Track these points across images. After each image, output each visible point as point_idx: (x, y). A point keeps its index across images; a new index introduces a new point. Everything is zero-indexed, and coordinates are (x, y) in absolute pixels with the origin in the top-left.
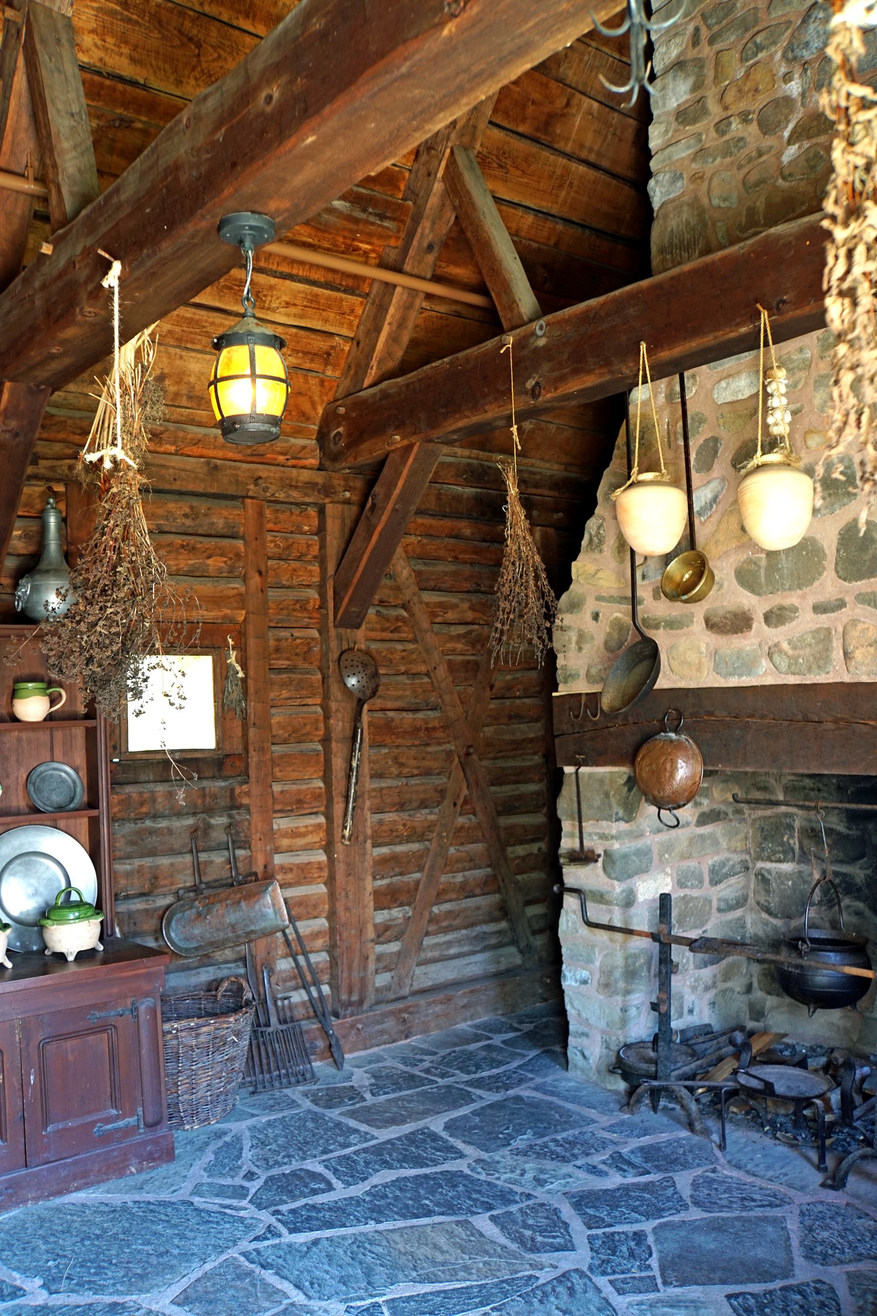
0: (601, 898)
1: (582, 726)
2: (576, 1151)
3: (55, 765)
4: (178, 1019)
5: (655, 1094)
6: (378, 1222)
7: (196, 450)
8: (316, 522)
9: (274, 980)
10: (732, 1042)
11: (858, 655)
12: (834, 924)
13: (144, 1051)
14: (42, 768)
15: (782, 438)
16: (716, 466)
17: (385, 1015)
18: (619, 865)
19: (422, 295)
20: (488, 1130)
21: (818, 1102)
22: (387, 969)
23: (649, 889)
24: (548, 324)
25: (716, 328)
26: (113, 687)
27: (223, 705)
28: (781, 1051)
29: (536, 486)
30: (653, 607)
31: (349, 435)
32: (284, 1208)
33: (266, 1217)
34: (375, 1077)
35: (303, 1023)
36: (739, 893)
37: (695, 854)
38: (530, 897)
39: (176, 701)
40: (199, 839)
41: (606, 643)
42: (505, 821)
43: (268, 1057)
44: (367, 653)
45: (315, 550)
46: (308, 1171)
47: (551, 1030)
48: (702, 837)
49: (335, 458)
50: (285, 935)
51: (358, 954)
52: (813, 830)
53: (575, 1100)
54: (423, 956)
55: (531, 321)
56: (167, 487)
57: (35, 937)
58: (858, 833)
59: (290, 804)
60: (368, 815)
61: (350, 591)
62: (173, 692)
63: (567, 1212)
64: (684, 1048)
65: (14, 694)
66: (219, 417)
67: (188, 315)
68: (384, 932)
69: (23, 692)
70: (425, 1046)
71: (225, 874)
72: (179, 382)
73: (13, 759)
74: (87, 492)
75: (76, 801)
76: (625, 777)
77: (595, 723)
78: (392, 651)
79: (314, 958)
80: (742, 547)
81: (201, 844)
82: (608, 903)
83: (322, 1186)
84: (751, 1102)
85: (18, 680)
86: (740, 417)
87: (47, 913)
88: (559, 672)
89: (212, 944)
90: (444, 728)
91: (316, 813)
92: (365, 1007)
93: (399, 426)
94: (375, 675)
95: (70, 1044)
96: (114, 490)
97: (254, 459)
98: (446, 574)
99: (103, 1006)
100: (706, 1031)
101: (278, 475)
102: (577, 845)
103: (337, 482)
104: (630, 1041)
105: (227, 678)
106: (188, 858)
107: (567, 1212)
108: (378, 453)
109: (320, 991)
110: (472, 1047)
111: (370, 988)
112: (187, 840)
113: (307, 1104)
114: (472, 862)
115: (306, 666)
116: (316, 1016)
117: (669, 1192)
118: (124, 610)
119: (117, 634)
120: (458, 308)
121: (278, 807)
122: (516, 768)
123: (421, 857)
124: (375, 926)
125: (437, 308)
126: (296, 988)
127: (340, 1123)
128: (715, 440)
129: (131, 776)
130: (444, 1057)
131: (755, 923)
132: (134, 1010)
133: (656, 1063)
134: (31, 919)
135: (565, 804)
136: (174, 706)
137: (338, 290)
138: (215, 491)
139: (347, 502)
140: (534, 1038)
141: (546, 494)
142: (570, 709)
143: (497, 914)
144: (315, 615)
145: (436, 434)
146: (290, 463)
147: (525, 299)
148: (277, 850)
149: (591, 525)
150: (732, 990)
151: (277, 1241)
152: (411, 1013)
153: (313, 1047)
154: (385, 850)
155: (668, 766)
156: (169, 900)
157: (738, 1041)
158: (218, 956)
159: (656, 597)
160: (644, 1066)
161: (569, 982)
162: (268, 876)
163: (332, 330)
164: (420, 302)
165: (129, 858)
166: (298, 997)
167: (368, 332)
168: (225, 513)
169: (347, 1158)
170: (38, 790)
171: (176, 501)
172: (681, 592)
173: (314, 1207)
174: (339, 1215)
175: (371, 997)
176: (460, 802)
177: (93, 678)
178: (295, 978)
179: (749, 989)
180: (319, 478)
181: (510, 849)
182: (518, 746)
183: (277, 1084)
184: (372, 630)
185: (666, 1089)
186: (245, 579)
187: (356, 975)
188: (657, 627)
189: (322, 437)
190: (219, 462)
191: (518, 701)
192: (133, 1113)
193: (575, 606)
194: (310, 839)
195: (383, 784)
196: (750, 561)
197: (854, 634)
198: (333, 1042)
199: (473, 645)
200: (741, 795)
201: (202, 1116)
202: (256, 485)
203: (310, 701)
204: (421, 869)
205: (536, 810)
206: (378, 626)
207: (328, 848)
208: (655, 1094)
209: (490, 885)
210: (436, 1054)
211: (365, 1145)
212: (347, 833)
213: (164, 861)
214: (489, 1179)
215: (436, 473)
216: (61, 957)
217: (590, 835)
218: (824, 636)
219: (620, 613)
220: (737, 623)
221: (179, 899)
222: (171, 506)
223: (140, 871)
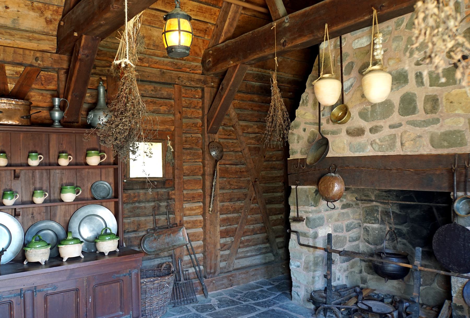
0: (305, 235)
1: (298, 171)
3: (102, 182)
4: (147, 277)
5: (325, 310)
7: (156, 66)
8: (201, 94)
9: (182, 264)
10: (355, 291)
11: (407, 144)
12: (395, 248)
13: (133, 290)
14: (97, 183)
15: (380, 60)
16: (352, 73)
17: (223, 278)
18: (312, 223)
19: (241, 8)
21: (389, 315)
22: (225, 260)
23: (323, 232)
24: (290, 18)
25: (356, 17)
26: (125, 149)
27: (165, 161)
28: (373, 296)
29: (282, 83)
30: (327, 126)
31: (213, 61)
34: (220, 301)
35: (193, 280)
36: (357, 235)
37: (340, 220)
38: (277, 235)
39: (149, 155)
40: (156, 211)
41: (308, 140)
42: (269, 206)
43: (180, 293)
44: (219, 143)
45: (200, 105)
47: (286, 285)
48: (343, 213)
49: (208, 70)
50: (187, 247)
51: (214, 255)
52: (386, 212)
53: (294, 311)
54: (238, 256)
55: (283, 17)
56: (145, 79)
57: (93, 246)
58: (404, 213)
59: (189, 198)
60: (218, 203)
61: (213, 120)
62: (148, 151)
64: (336, 293)
65: (86, 155)
66: (166, 46)
67: (153, 13)
68: (223, 247)
69: (90, 154)
70: (238, 290)
71: (165, 224)
72: (150, 39)
73: (86, 179)
74: (115, 77)
75: (110, 195)
76: (315, 190)
77: (303, 170)
78: (228, 143)
79: (198, 256)
80: (361, 104)
81: (156, 212)
82: (307, 237)
84: (363, 315)
85: (88, 150)
86: (363, 54)
87: (98, 237)
88: (290, 151)
89: (160, 250)
90: (247, 171)
91: (199, 202)
92: (216, 275)
93: (232, 58)
94: (222, 151)
95: (105, 287)
96: (126, 75)
97: (178, 70)
98: (248, 114)
99: (118, 272)
100: (344, 287)
101: (187, 76)
102: (296, 215)
103: (209, 79)
104: (315, 290)
105: (167, 151)
108: (224, 68)
109: (199, 268)
110: (256, 291)
111: (218, 267)
112: (151, 211)
113: (194, 311)
114: (256, 221)
115: (196, 147)
116: (198, 278)
118: (130, 121)
119: (127, 129)
120: (255, 13)
121: (185, 199)
122: (273, 187)
123: (238, 219)
124: (220, 244)
125: (247, 13)
126: (191, 267)
128: (352, 63)
129: (131, 187)
130: (245, 294)
131: (363, 247)
132: (130, 274)
133: (326, 298)
134: (91, 240)
135: (292, 200)
136: (147, 161)
137: (210, 5)
138: (163, 81)
139: (212, 87)
140: (278, 288)
141: (287, 86)
142: (294, 164)
143: (265, 241)
144: (200, 129)
145: (246, 61)
146: (191, 72)
147: (281, 8)
148: (185, 215)
149: (304, 96)
152: (233, 277)
153: (197, 289)
154: (224, 216)
155: (331, 186)
156: (144, 233)
157: (357, 292)
158: (162, 254)
159: (328, 122)
160: (321, 299)
161: (293, 266)
162: (181, 225)
163: (208, 21)
164: (241, 11)
165: (129, 217)
166: (192, 270)
167: (221, 22)
168: (167, 90)
170: (95, 191)
171: (149, 85)
172: (338, 120)
175: (218, 271)
176: (252, 199)
177: (117, 146)
178: (190, 263)
179: (361, 272)
180: (202, 78)
181: (270, 217)
182: (274, 179)
183: (183, 303)
184: (221, 135)
185: (330, 308)
186: (174, 115)
187: (213, 262)
188: (328, 134)
189: (203, 62)
190: (165, 70)
191: (274, 162)
193: (297, 126)
194: (197, 211)
195: (224, 191)
196: (365, 109)
197: (405, 136)
198: (204, 288)
199: (258, 141)
200: (359, 198)
201: (154, 315)
202: (179, 79)
203: (197, 160)
204: (237, 224)
205: (280, 203)
206: (223, 133)
207: (204, 215)
208: (325, 310)
209: (263, 230)
210: (242, 293)
212: (211, 209)
213: (143, 219)
215: (245, 77)
216: (103, 254)
217: (301, 211)
218: (393, 138)
219: (314, 129)
220: (359, 132)
221: (148, 233)
222: (147, 86)
223: (133, 222)
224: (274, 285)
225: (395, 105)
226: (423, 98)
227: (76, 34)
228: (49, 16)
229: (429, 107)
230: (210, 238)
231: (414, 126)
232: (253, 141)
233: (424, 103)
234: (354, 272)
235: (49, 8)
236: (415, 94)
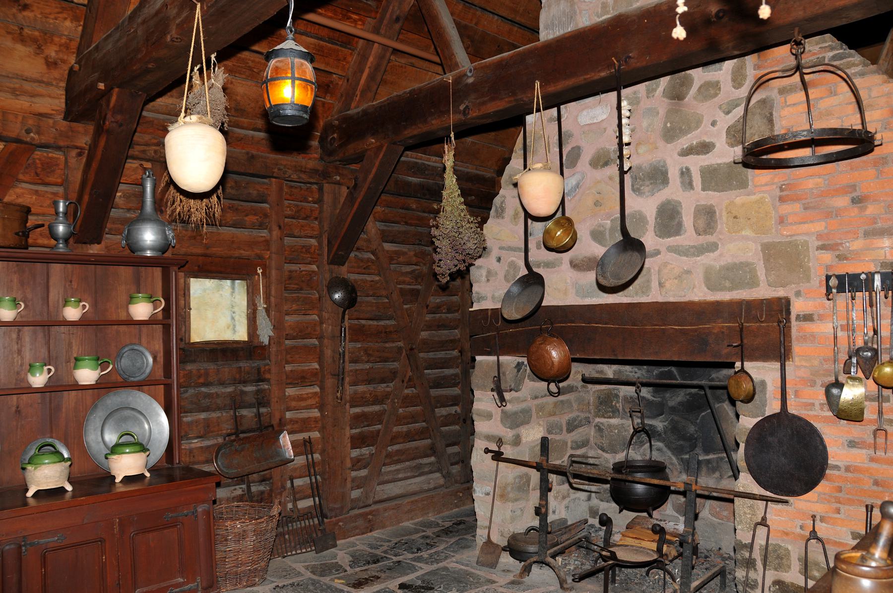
11: (668, 285)
17: (357, 516)
19: (391, 50)
24: (475, 69)
30: (538, 254)
34: (352, 556)
42: (434, 392)
49: (330, 153)
54: (381, 478)
68: (358, 463)
70: (384, 537)
106: (226, 415)
113: (309, 574)
124: (351, 459)
143: (429, 452)
148: (289, 409)
149: (497, 200)
154: (358, 410)
176: (406, 380)
186: (270, 231)
192: (194, 580)
194: (309, 402)
213: (215, 415)
225: (649, 219)
226: (693, 210)
227: (101, 86)
228: (53, 54)
229: (701, 223)
230: (334, 448)
231: (679, 254)
232: (407, 279)
233: (695, 217)
234: (579, 499)
235: (52, 40)
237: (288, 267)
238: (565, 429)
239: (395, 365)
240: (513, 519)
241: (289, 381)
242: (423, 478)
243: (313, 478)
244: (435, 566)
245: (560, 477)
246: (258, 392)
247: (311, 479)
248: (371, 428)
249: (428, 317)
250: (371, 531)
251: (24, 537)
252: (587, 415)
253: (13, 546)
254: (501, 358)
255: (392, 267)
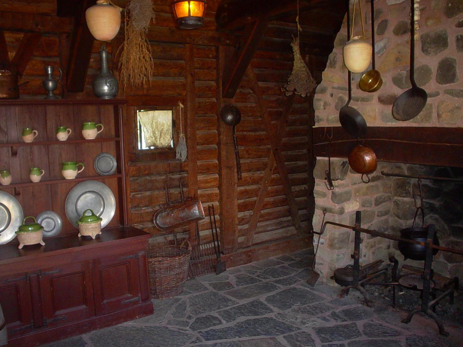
0: (330, 211)
2: (317, 311)
6: (240, 337)
11: (444, 116)
20: (284, 301)
22: (243, 235)
32: (203, 331)
33: (196, 334)
42: (290, 176)
46: (212, 316)
47: (308, 261)
54: (257, 230)
63: (314, 336)
68: (242, 221)
82: (333, 213)
83: (218, 322)
106: (162, 193)
107: (314, 336)
113: (211, 289)
117: (354, 329)
124: (238, 218)
127: (224, 297)
148: (199, 188)
149: (331, 56)
150: (382, 248)
151: (201, 343)
154: (242, 188)
169: (227, 311)
173: (214, 330)
174: (225, 333)
179: (389, 247)
186: (186, 78)
193: (323, 91)
194: (212, 184)
204: (257, 196)
205: (305, 171)
207: (220, 187)
210: (262, 269)
211: (234, 306)
213: (156, 192)
214: (284, 321)
224: (295, 260)
225: (432, 71)
236: (455, 60)
237: (197, 100)
238: (373, 204)
239: (266, 160)
240: (338, 260)
241: (200, 171)
242: (284, 229)
243: (214, 230)
244: (288, 287)
245: (369, 235)
246: (180, 179)
247: (212, 231)
248: (250, 199)
249: (287, 129)
250: (250, 262)
251: (40, 270)
252: (390, 195)
253: (34, 275)
254: (331, 159)
255: (264, 97)
